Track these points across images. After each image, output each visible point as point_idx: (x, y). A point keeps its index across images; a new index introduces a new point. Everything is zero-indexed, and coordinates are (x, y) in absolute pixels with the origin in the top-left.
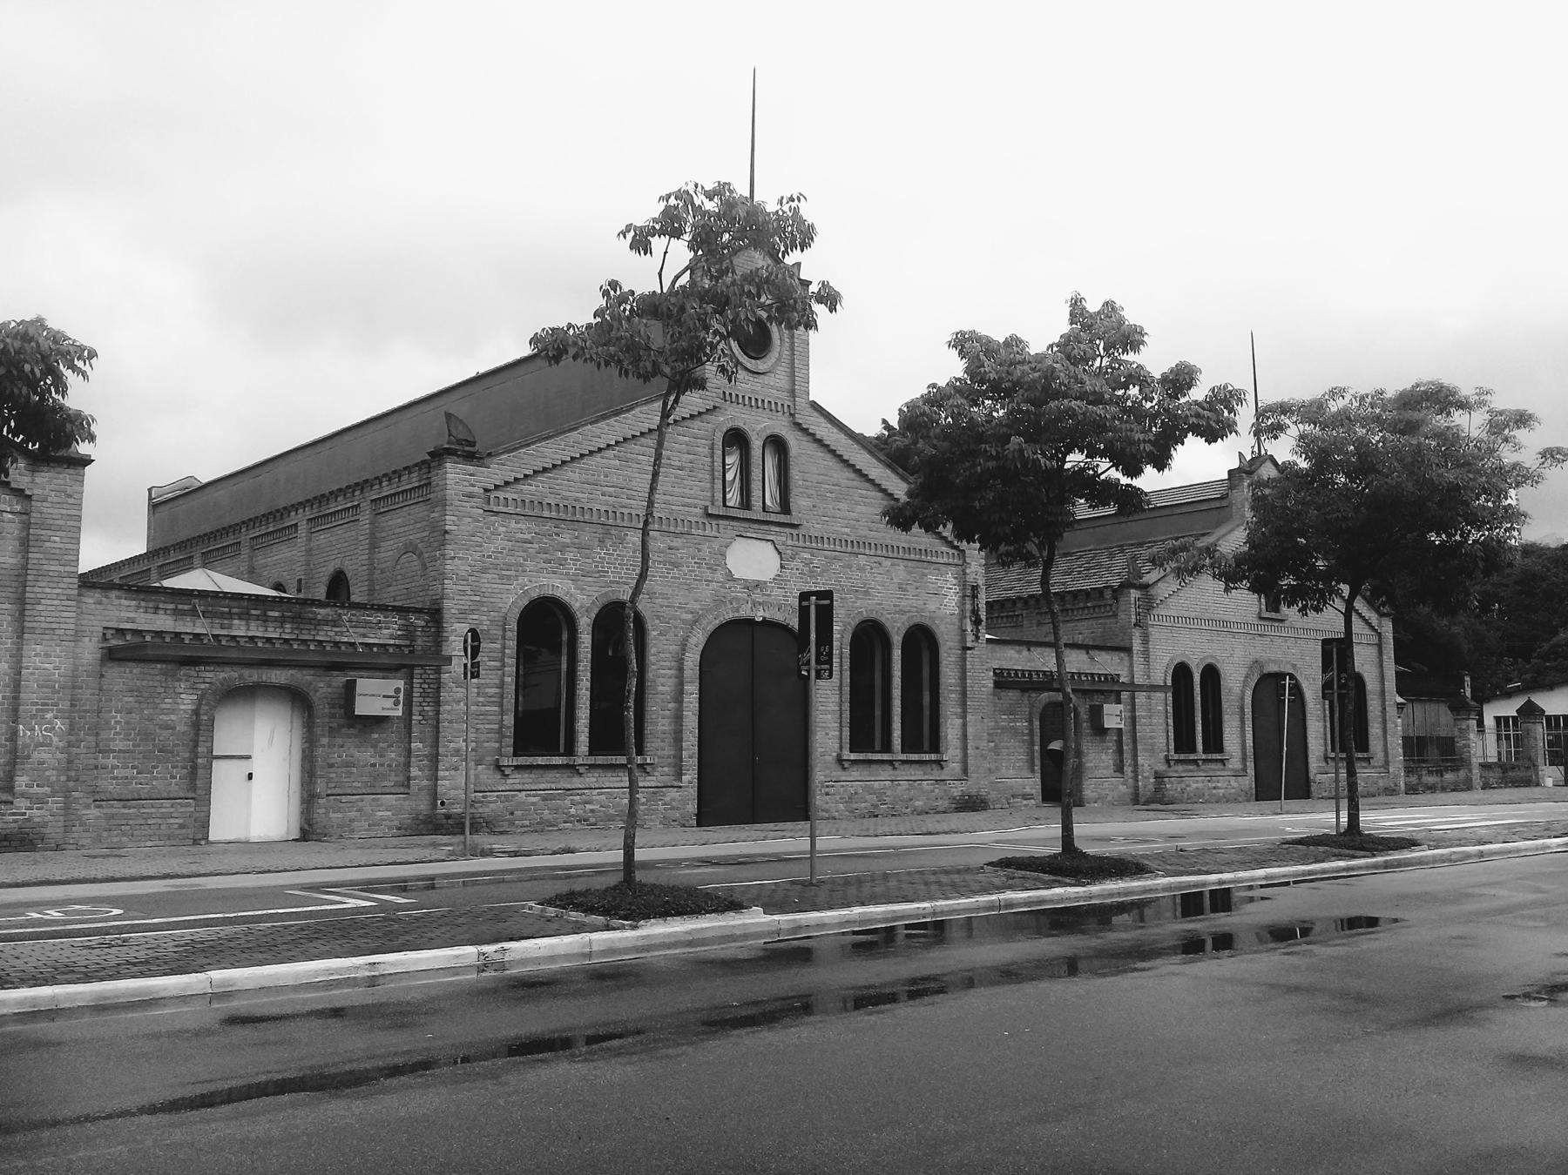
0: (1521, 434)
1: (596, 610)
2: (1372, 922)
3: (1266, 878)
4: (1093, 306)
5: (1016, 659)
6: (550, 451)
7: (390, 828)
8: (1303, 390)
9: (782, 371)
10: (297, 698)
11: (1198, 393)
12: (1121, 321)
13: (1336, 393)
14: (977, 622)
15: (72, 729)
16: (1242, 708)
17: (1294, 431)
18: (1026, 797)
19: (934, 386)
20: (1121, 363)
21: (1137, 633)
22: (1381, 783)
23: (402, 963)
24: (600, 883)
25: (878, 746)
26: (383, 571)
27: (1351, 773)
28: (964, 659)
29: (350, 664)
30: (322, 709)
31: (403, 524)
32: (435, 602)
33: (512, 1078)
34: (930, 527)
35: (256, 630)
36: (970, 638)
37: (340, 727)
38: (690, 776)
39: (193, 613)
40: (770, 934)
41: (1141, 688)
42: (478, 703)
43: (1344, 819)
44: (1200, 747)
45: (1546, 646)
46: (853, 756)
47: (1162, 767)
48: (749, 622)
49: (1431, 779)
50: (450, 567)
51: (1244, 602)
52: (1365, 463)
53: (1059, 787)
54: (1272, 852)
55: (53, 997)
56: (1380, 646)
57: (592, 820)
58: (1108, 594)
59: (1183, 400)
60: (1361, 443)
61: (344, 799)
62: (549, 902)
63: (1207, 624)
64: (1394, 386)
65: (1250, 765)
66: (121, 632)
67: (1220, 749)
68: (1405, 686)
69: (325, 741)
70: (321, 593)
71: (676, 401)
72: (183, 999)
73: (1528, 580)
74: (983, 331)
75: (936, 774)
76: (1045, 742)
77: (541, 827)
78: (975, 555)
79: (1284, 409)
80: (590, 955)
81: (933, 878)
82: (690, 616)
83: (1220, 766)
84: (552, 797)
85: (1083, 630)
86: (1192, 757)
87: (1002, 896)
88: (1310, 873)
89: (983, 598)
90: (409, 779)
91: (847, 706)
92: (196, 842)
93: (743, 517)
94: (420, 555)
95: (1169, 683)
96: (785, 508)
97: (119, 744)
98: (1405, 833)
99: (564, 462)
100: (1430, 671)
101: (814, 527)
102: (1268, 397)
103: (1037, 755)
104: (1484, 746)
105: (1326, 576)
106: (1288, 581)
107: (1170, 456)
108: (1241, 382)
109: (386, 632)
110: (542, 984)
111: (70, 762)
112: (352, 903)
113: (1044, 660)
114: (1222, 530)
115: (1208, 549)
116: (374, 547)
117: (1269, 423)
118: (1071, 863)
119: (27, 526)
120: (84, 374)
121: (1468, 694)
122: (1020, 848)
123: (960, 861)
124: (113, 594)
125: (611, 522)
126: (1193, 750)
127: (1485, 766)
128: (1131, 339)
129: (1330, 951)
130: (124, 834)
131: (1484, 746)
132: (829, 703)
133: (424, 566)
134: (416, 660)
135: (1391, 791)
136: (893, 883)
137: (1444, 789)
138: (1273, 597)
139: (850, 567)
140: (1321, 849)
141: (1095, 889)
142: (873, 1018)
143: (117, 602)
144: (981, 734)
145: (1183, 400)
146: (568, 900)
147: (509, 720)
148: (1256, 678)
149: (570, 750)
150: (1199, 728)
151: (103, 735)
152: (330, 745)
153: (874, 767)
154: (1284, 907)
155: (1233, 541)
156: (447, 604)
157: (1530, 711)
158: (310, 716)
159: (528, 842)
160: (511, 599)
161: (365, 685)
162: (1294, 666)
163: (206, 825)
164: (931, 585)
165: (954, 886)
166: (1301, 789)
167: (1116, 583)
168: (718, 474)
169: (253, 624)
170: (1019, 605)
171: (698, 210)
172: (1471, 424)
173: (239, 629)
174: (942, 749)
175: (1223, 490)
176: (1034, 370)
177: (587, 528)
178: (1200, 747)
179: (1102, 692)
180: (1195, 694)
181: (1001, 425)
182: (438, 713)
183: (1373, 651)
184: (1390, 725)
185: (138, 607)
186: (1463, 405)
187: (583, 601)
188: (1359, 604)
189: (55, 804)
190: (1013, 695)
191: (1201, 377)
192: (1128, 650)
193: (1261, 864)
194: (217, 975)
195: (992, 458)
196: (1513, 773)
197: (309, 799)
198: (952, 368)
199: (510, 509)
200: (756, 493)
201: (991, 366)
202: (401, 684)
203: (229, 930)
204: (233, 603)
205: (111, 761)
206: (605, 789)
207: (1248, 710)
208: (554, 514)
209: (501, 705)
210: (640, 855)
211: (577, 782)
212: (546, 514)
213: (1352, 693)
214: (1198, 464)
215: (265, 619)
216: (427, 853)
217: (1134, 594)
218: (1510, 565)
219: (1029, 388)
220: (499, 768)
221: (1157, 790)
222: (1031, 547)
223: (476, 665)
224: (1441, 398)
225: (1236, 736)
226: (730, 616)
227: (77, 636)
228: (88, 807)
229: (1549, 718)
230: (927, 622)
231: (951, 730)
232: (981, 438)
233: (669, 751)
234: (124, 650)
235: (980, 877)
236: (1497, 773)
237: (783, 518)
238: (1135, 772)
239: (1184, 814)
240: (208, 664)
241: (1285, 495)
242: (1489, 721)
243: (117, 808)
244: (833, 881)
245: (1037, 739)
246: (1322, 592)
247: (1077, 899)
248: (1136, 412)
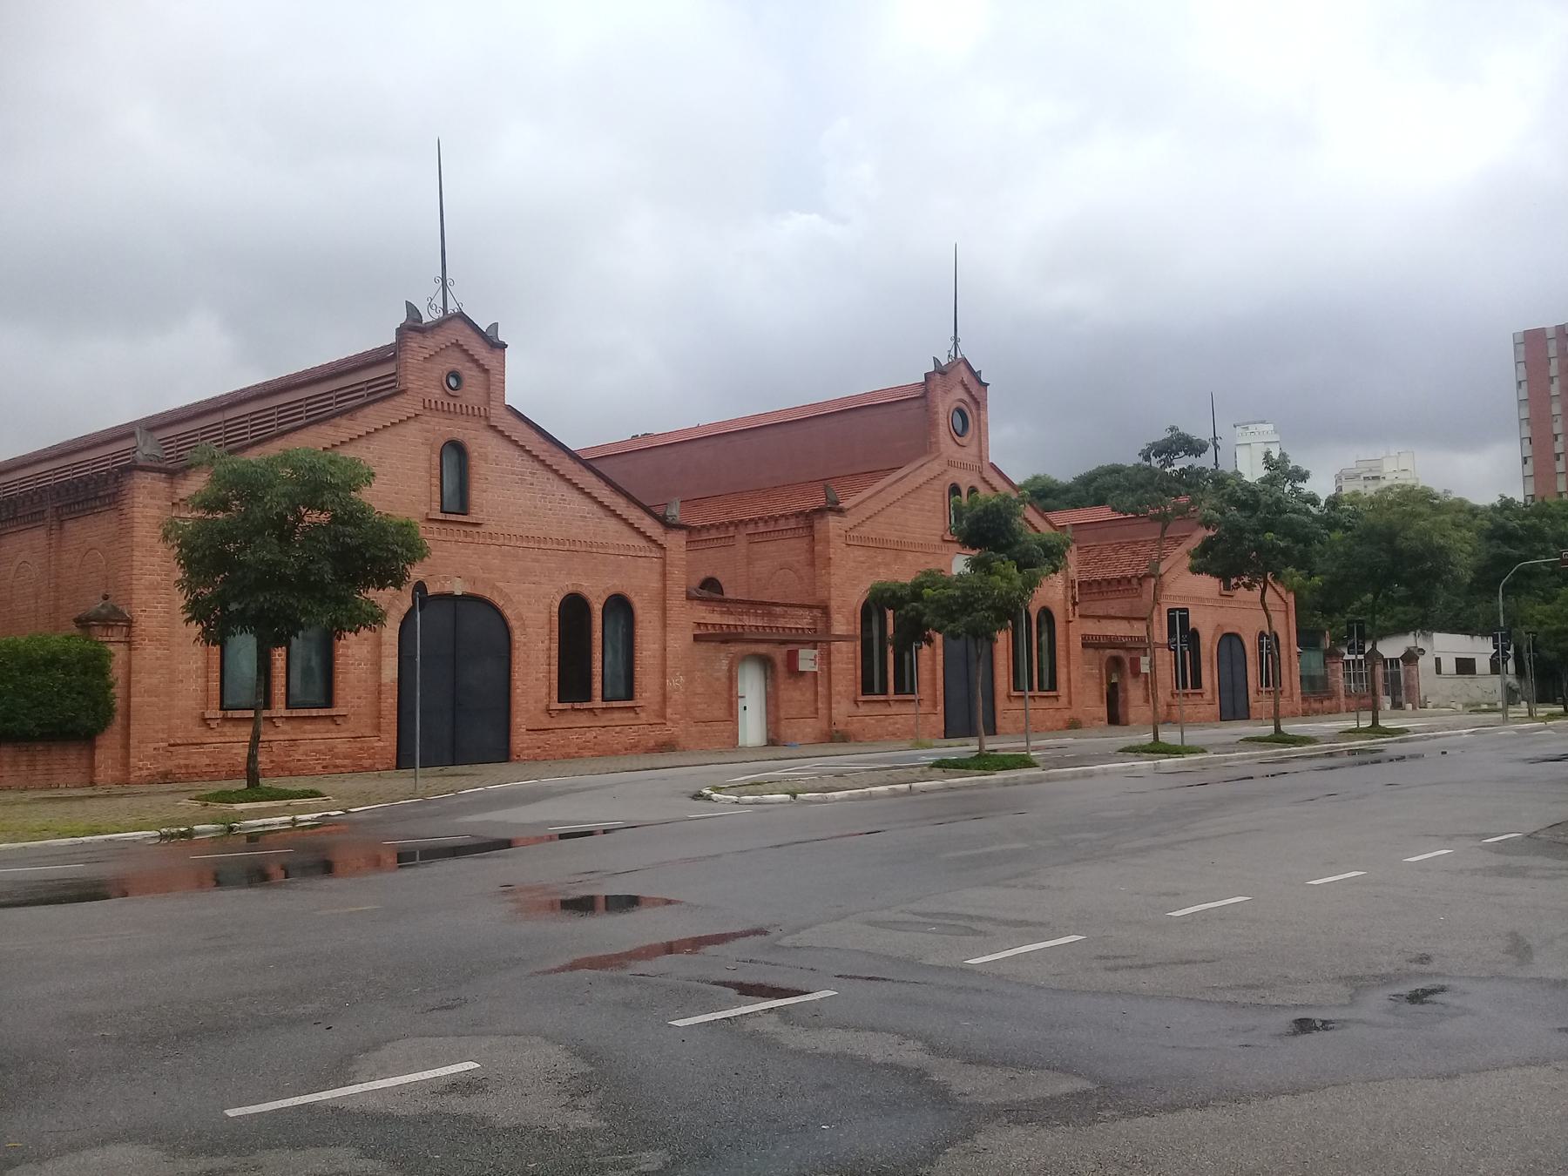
5: (1092, 628)
9: (975, 442)
12: (1474, 511)
25: (877, 689)
38: (940, 708)
44: (891, 689)
45: (1357, 604)
47: (1169, 699)
49: (1316, 706)
58: (1134, 581)
75: (1056, 705)
76: (1109, 677)
83: (632, 715)
85: (1116, 606)
95: (859, 631)
97: (700, 690)
119: (664, 565)
134: (821, 639)
156: (833, 603)
157: (1374, 656)
167: (1141, 573)
173: (749, 621)
183: (1283, 615)
190: (1091, 651)
206: (902, 714)
211: (889, 711)
221: (1169, 714)
233: (929, 692)
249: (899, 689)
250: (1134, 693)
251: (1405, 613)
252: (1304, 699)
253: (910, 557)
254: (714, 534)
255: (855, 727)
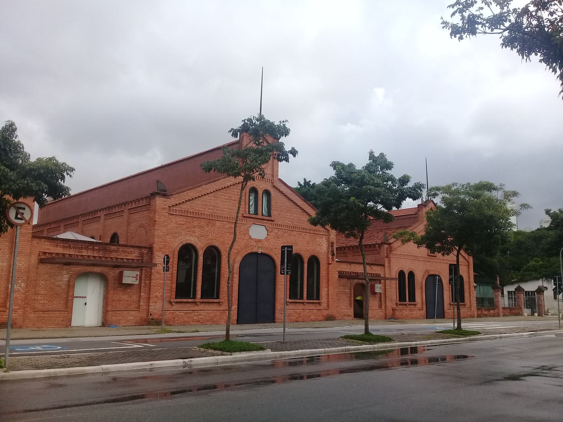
0: (514, 199)
1: (205, 249)
2: (465, 357)
3: (431, 343)
4: (377, 154)
5: (346, 268)
6: (192, 194)
7: (133, 323)
8: (442, 184)
10: (103, 277)
11: (410, 185)
12: (386, 160)
13: (453, 184)
14: (333, 255)
15: (27, 286)
16: (422, 287)
17: (440, 196)
18: (349, 316)
19: (326, 179)
20: (386, 173)
21: (387, 260)
22: (469, 313)
23: (160, 364)
24: (217, 341)
25: (299, 297)
26: (131, 233)
27: (458, 309)
28: (328, 268)
29: (121, 266)
30: (111, 281)
31: (139, 218)
32: (151, 245)
33: (211, 394)
34: (323, 226)
35: (90, 253)
36: (331, 260)
37: (117, 287)
39: (70, 247)
40: (273, 358)
41: (387, 279)
42: (163, 280)
43: (456, 325)
44: (407, 299)
45: (525, 267)
46: (290, 301)
47: (395, 306)
48: (256, 253)
49: (486, 312)
50: (156, 233)
51: (424, 250)
52: (463, 207)
53: (360, 312)
54: (432, 335)
55: (55, 372)
56: (468, 266)
57: (201, 321)
58: (377, 246)
59: (405, 187)
60: (463, 201)
61: (118, 312)
62: (202, 347)
63: (410, 258)
64: (474, 181)
65: (425, 306)
66: (45, 253)
67: (414, 301)
68: (477, 280)
69: (112, 292)
70: (108, 240)
71: (246, 184)
72: (94, 374)
73: (519, 244)
74: (341, 161)
75: (318, 307)
76: (355, 296)
77: (184, 323)
78: (333, 233)
79: (438, 189)
80: (217, 363)
81: (323, 341)
82: (236, 251)
83: (414, 306)
84: (188, 313)
86: (405, 303)
87: (346, 347)
88: (445, 342)
89: (335, 246)
90: (140, 306)
91: (288, 283)
92: (67, 326)
93: (255, 217)
94: (145, 228)
96: (269, 214)
97: (42, 292)
98: (475, 330)
99: (196, 198)
100: (486, 274)
101: (279, 221)
102: (432, 184)
103: (353, 301)
104: (504, 302)
105: (452, 243)
106: (438, 245)
107: (401, 204)
108: (424, 182)
109: (134, 255)
110: (207, 371)
111: (26, 298)
112: (136, 346)
113: (359, 269)
114: (415, 225)
115: (412, 233)
116: (128, 224)
117: (433, 192)
118: (367, 337)
120: (71, 176)
121: (498, 283)
122: (348, 332)
123: (331, 336)
124: (43, 240)
125: (211, 218)
126: (405, 301)
127: (504, 308)
128: (389, 166)
129: (451, 365)
130: (43, 323)
131: (504, 302)
132: (282, 282)
133: (147, 232)
134: (144, 265)
135: (472, 316)
136: (310, 343)
137: (490, 316)
138: (431, 248)
139: (291, 235)
140: (449, 334)
141: (376, 346)
142: (314, 381)
143: (44, 243)
144: (335, 293)
145: (405, 187)
146: (208, 346)
147: (174, 286)
148: (426, 276)
149: (194, 297)
150: (407, 293)
151: (37, 289)
152: (113, 294)
153: (297, 304)
154: (436, 352)
155: (420, 230)
156: (155, 246)
157: (519, 289)
158: (107, 283)
159: (182, 328)
160: (177, 244)
161: (126, 273)
162: (439, 272)
163: (70, 320)
164: (318, 243)
165: (330, 344)
166: (442, 315)
167: (379, 242)
168: (247, 203)
169: (89, 251)
170: (347, 249)
171: (255, 124)
172: (498, 195)
173: (85, 253)
174: (320, 299)
175: (416, 211)
176: (358, 175)
177: (203, 220)
178: (407, 299)
179: (375, 280)
180: (406, 282)
181: (347, 193)
182: (150, 283)
183: (466, 267)
184: (472, 293)
185: (51, 245)
186: (495, 189)
187: (201, 246)
188: (462, 252)
189: (20, 312)
190: (344, 280)
191: (411, 179)
192: (383, 265)
193: (429, 339)
194: (104, 366)
195: (344, 203)
196: (513, 311)
197: (105, 312)
198: (331, 173)
199: (177, 213)
200: (260, 210)
201: (344, 173)
202: (138, 273)
203: (99, 354)
204: (83, 244)
205: (39, 298)
206: (208, 310)
207: (424, 287)
208: (192, 215)
209: (172, 281)
210: (231, 333)
211: (196, 308)
212: (189, 215)
213: (459, 283)
214: (409, 204)
215: (93, 250)
216: (148, 331)
217: (386, 246)
218: (510, 241)
219: (356, 181)
220: (170, 302)
221: (393, 314)
222: (356, 232)
223: (168, 267)
224: (489, 187)
225: (420, 296)
226: (250, 251)
227: (30, 254)
228: (31, 313)
229: (526, 292)
230: (316, 255)
231: (323, 292)
232: (341, 197)
233: (326, 300)
234: (46, 260)
235: (338, 341)
236: (508, 311)
237: (268, 218)
238: (386, 308)
239: (402, 323)
240: (74, 265)
241: (437, 217)
242: (506, 293)
243: (41, 314)
244: (290, 342)
245: (353, 295)
246: (449, 249)
247: (370, 349)
248: (390, 189)
249: (310, 297)
250: (373, 304)
251: (546, 271)
252: (478, 309)
253: (218, 224)
254: (117, 209)
255: (168, 316)
